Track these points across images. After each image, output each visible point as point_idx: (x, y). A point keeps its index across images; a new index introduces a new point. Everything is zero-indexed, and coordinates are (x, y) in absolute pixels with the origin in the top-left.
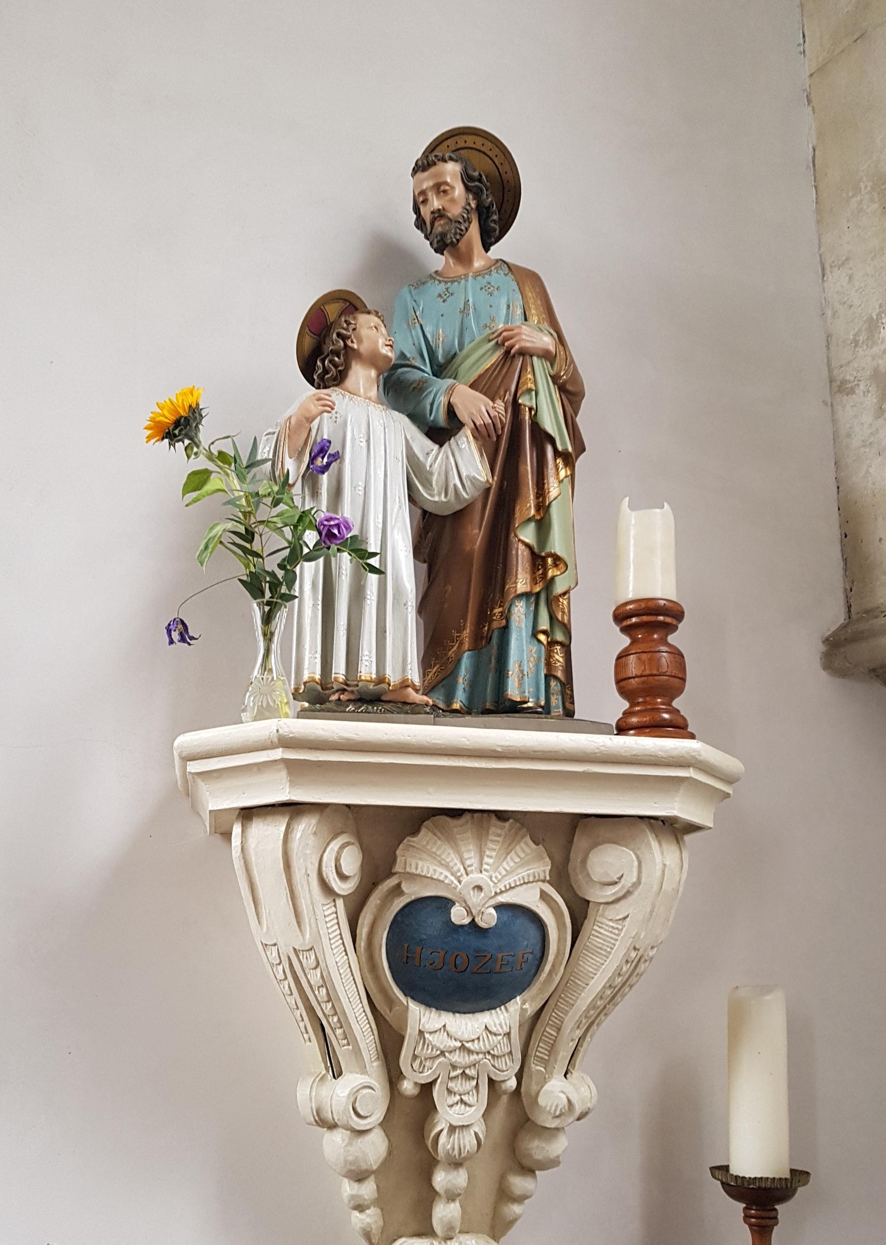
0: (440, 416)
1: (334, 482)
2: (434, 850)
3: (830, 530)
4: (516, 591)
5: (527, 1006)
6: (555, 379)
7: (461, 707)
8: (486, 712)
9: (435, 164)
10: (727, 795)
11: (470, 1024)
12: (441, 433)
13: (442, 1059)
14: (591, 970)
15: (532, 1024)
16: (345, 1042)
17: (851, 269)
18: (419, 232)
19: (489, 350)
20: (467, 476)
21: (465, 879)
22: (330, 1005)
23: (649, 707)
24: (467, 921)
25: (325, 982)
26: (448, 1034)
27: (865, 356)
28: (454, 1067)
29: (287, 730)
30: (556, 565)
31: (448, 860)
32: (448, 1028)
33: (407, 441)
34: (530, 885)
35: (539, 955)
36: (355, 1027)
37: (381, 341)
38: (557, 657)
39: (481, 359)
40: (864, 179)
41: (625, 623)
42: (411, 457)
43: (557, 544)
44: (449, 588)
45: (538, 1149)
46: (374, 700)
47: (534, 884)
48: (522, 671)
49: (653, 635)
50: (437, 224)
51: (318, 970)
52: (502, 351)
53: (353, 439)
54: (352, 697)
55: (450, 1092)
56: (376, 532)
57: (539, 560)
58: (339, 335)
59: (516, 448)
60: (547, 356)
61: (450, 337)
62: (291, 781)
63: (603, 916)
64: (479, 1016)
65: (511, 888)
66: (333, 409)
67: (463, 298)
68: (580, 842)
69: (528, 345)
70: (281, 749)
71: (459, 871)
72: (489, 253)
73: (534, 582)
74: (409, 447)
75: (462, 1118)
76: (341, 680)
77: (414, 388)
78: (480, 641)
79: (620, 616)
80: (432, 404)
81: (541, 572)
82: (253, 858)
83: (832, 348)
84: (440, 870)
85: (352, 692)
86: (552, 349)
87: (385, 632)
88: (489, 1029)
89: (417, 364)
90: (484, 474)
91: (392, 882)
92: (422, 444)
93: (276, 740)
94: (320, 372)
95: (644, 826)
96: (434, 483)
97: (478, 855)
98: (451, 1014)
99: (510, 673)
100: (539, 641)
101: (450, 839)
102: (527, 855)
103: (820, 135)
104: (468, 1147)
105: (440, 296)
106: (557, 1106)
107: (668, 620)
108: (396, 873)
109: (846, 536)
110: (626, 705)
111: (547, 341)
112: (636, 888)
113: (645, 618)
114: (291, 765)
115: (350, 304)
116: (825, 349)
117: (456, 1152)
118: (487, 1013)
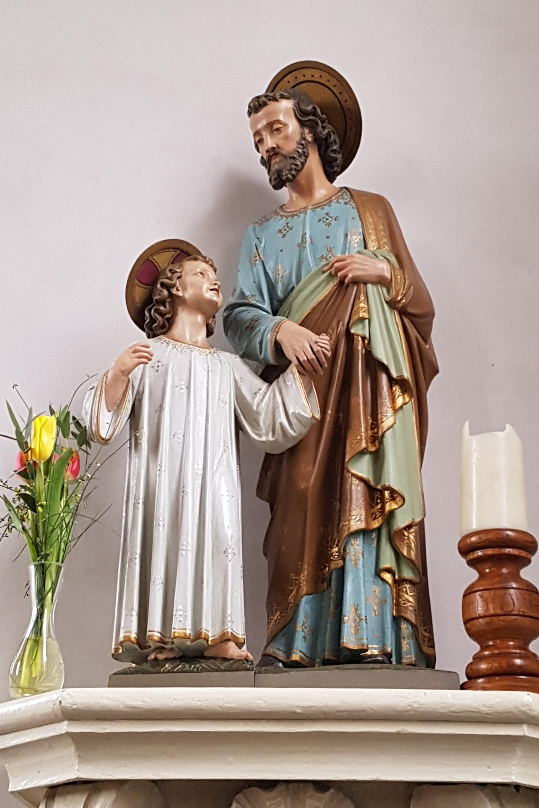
0: (268, 353)
4: (349, 528)
6: (392, 304)
7: (301, 658)
8: (326, 663)
9: (265, 104)
12: (271, 373)
18: (264, 168)
19: (323, 282)
20: (293, 413)
23: (496, 652)
29: (70, 701)
30: (393, 499)
33: (235, 381)
37: (205, 286)
38: (406, 596)
39: (314, 292)
41: (471, 556)
42: (240, 398)
43: (392, 478)
46: (195, 658)
48: (359, 616)
50: (273, 161)
53: (174, 387)
54: (171, 655)
56: (194, 479)
57: (375, 494)
58: (163, 285)
60: (382, 282)
61: (288, 271)
62: (79, 756)
66: (150, 360)
67: (302, 231)
69: (360, 273)
70: (66, 723)
72: (334, 184)
73: (371, 516)
74: (237, 389)
76: (156, 638)
77: (247, 328)
79: (465, 550)
80: (261, 343)
81: (379, 506)
85: (171, 650)
86: (388, 275)
87: (202, 583)
89: (254, 302)
90: (309, 411)
92: (251, 383)
93: (59, 713)
94: (148, 321)
95: (480, 794)
96: (261, 423)
99: (346, 618)
100: (383, 580)
105: (280, 231)
107: (523, 554)
110: (475, 647)
111: (383, 268)
113: (490, 552)
114: (78, 739)
115: (181, 251)
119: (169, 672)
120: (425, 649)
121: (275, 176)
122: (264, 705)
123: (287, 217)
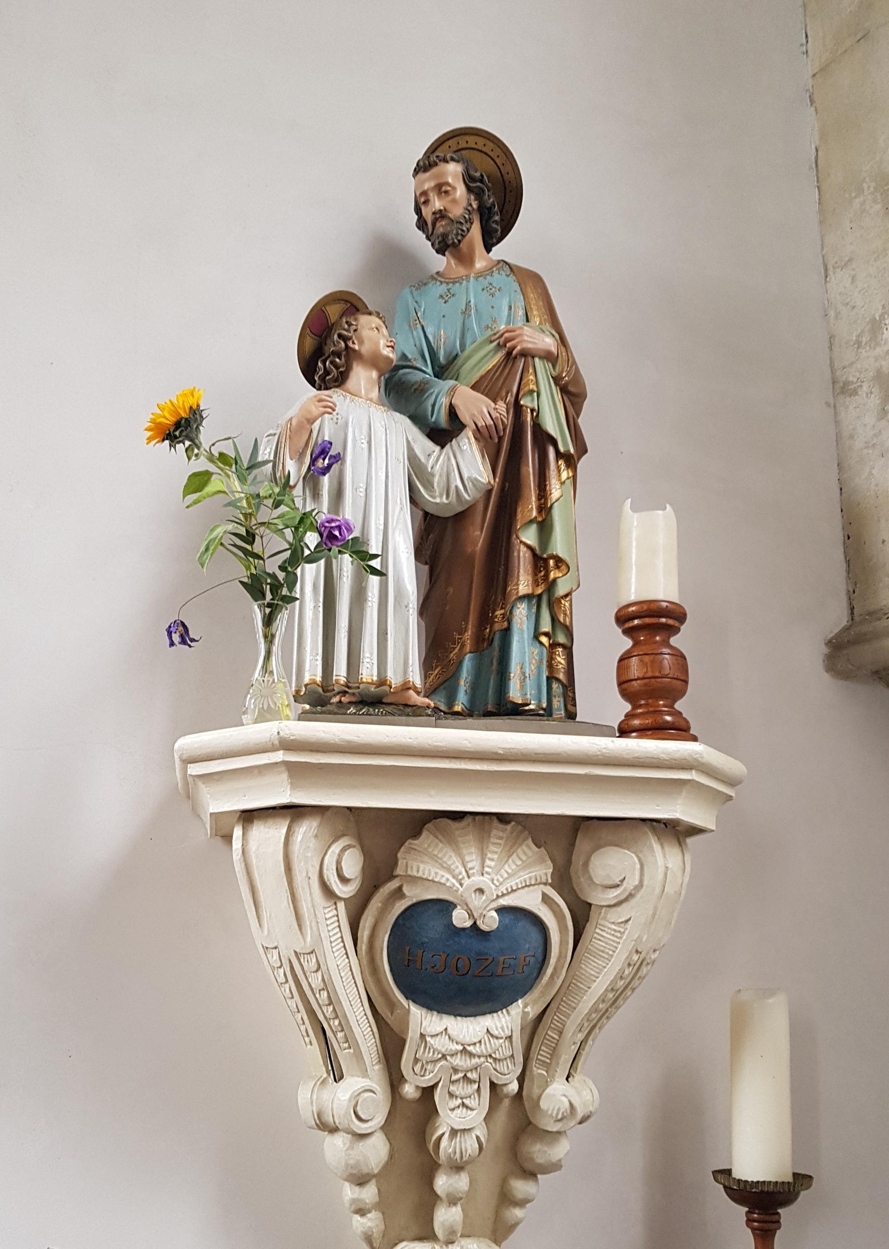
0: (441, 418)
1: (335, 484)
2: (436, 853)
3: (833, 532)
4: (518, 593)
5: (528, 1009)
6: (557, 380)
7: (463, 710)
8: (488, 714)
9: (436, 164)
10: (730, 798)
11: (471, 1028)
12: (442, 434)
13: (443, 1062)
14: (593, 973)
15: (534, 1028)
16: (346, 1045)
17: (854, 269)
18: (421, 233)
19: (490, 351)
20: (469, 478)
21: (466, 882)
22: (331, 1008)
23: (651, 709)
24: (468, 924)
25: (327, 985)
26: (449, 1038)
27: (868, 357)
28: (456, 1070)
29: (288, 732)
30: (557, 567)
31: (449, 863)
32: (450, 1031)
33: (408, 442)
34: (532, 888)
35: (540, 958)
36: (356, 1030)
37: (382, 342)
38: (559, 659)
39: (483, 361)
40: (867, 179)
41: (627, 625)
42: (413, 459)
43: (559, 546)
44: (451, 590)
45: (539, 1152)
46: (375, 702)
47: (536, 887)
48: (524, 674)
49: (655, 637)
50: (438, 225)
51: (320, 973)
52: (504, 352)
53: (354, 440)
54: (353, 699)
55: (451, 1095)
56: (377, 534)
57: (541, 562)
58: (340, 336)
59: (518, 449)
60: (549, 357)
61: (452, 338)
62: (292, 784)
63: (605, 919)
64: (480, 1019)
65: (513, 891)
66: (334, 410)
67: (465, 299)
68: (582, 845)
69: (530, 346)
70: (282, 752)
71: (460, 873)
72: (491, 254)
73: (536, 583)
74: (410, 449)
75: (464, 1121)
76: (342, 682)
77: (416, 390)
78: (482, 643)
79: (622, 618)
80: (433, 406)
81: (542, 573)
82: (253, 861)
83: (835, 349)
84: (441, 873)
85: (353, 694)
86: (554, 350)
87: (387, 634)
88: (491, 1032)
89: (418, 365)
90: (485, 476)
91: (393, 885)
92: (423, 445)
93: (277, 742)
94: (321, 373)
95: (646, 828)
96: (435, 484)
97: (479, 858)
98: (452, 1017)
99: (512, 675)
100: (541, 643)
101: (451, 841)
102: (529, 858)
103: (823, 136)
104: (469, 1151)
105: (441, 296)
106: (559, 1110)
107: (671, 622)
108: (397, 876)
109: (849, 538)
110: (628, 707)
111: (549, 342)
112: (638, 891)
113: (647, 620)
114: (292, 768)
115: (351, 305)
116: (828, 350)
117: (458, 1156)
118: (489, 1017)
119: (355, 714)
120: (570, 707)
121: (440, 239)
122: (469, 745)
123: (448, 283)
